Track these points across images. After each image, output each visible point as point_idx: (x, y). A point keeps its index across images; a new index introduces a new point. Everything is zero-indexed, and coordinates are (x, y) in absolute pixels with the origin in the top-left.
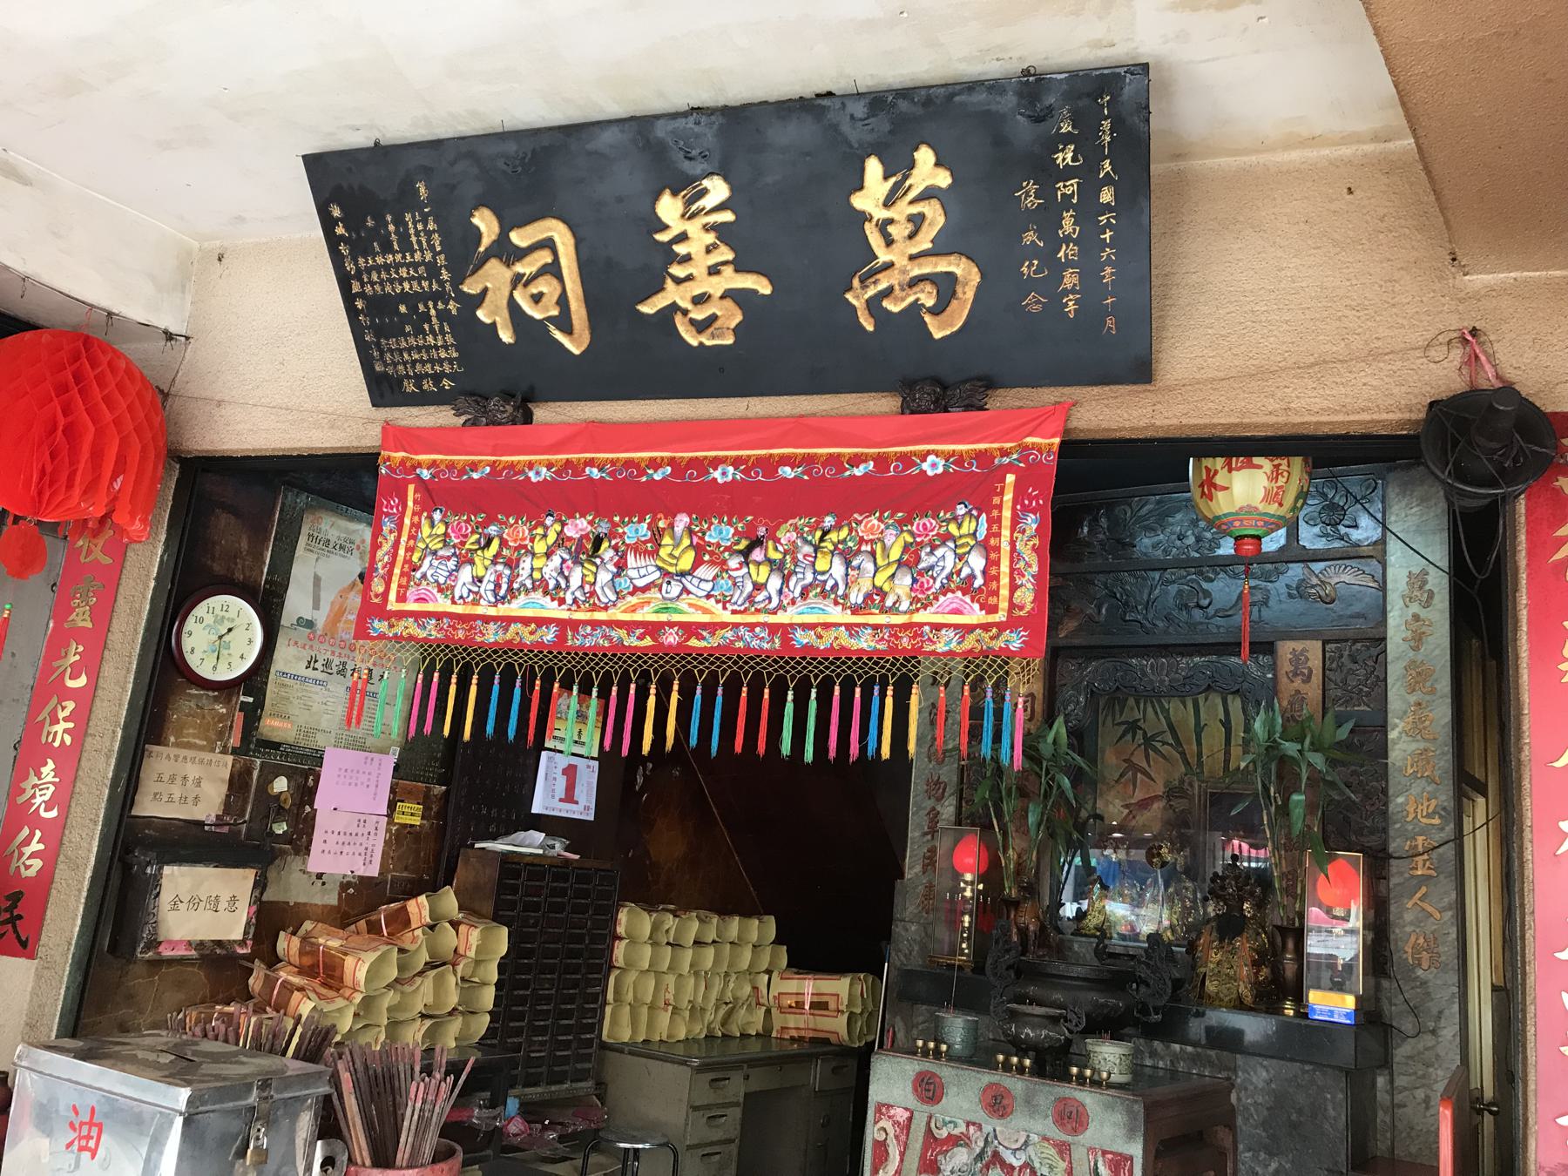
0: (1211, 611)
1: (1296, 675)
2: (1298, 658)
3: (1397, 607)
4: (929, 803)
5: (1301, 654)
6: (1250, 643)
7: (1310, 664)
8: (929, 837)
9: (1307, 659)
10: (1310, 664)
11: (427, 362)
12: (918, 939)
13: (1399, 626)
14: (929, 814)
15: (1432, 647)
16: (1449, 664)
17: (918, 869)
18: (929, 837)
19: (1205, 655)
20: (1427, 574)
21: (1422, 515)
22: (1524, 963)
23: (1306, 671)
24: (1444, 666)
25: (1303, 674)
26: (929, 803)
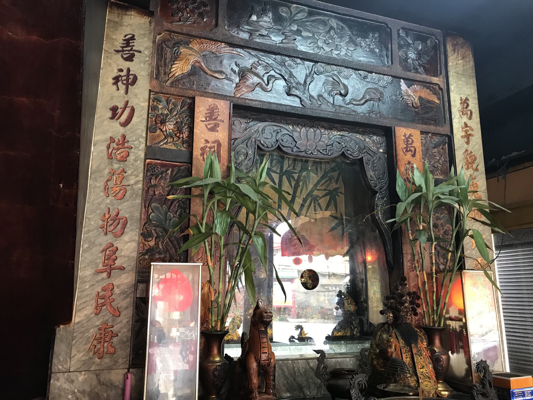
0: (348, 98)
1: (407, 151)
2: (408, 139)
3: (456, 117)
4: (105, 240)
5: (409, 137)
6: (298, 318)
7: (414, 145)
8: (105, 275)
9: (413, 141)
10: (414, 145)
11: (407, 145)
12: (88, 389)
13: (458, 128)
14: (104, 250)
15: (474, 143)
16: (483, 154)
17: (89, 310)
18: (105, 275)
19: (340, 131)
20: (468, 100)
21: (463, 66)
22: (396, 155)
23: (413, 149)
24: (480, 155)
25: (411, 150)
26: (105, 240)
